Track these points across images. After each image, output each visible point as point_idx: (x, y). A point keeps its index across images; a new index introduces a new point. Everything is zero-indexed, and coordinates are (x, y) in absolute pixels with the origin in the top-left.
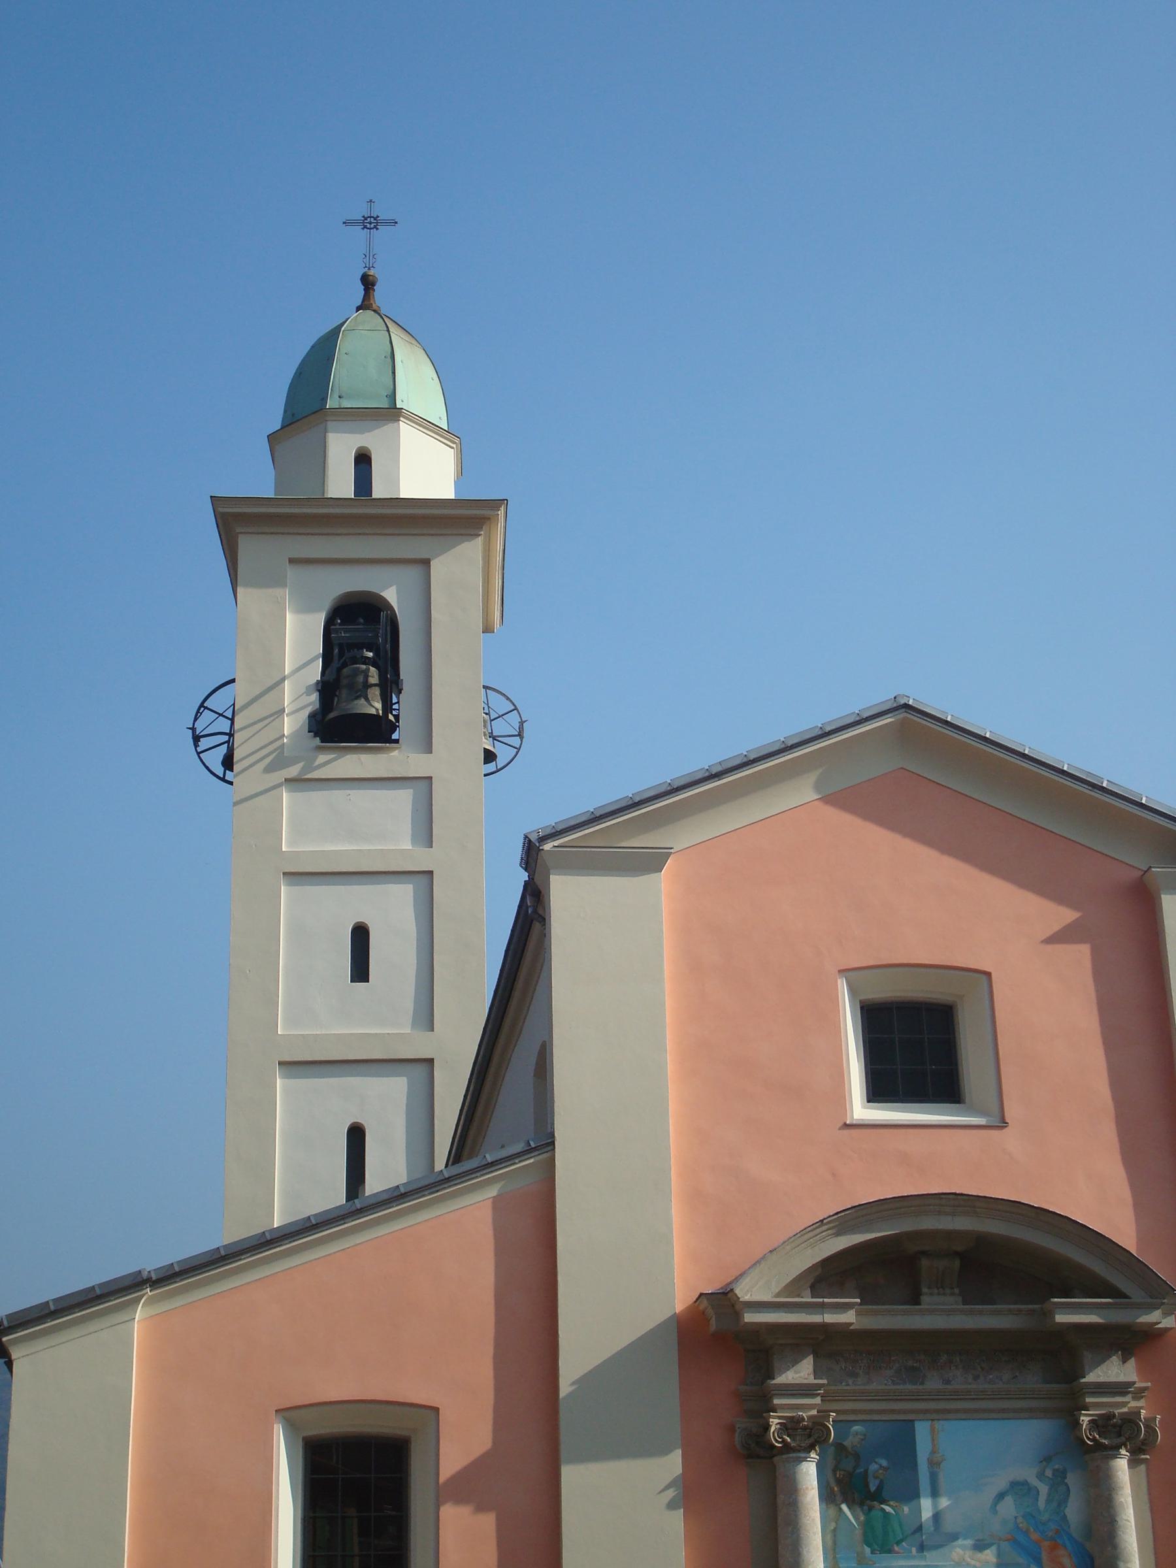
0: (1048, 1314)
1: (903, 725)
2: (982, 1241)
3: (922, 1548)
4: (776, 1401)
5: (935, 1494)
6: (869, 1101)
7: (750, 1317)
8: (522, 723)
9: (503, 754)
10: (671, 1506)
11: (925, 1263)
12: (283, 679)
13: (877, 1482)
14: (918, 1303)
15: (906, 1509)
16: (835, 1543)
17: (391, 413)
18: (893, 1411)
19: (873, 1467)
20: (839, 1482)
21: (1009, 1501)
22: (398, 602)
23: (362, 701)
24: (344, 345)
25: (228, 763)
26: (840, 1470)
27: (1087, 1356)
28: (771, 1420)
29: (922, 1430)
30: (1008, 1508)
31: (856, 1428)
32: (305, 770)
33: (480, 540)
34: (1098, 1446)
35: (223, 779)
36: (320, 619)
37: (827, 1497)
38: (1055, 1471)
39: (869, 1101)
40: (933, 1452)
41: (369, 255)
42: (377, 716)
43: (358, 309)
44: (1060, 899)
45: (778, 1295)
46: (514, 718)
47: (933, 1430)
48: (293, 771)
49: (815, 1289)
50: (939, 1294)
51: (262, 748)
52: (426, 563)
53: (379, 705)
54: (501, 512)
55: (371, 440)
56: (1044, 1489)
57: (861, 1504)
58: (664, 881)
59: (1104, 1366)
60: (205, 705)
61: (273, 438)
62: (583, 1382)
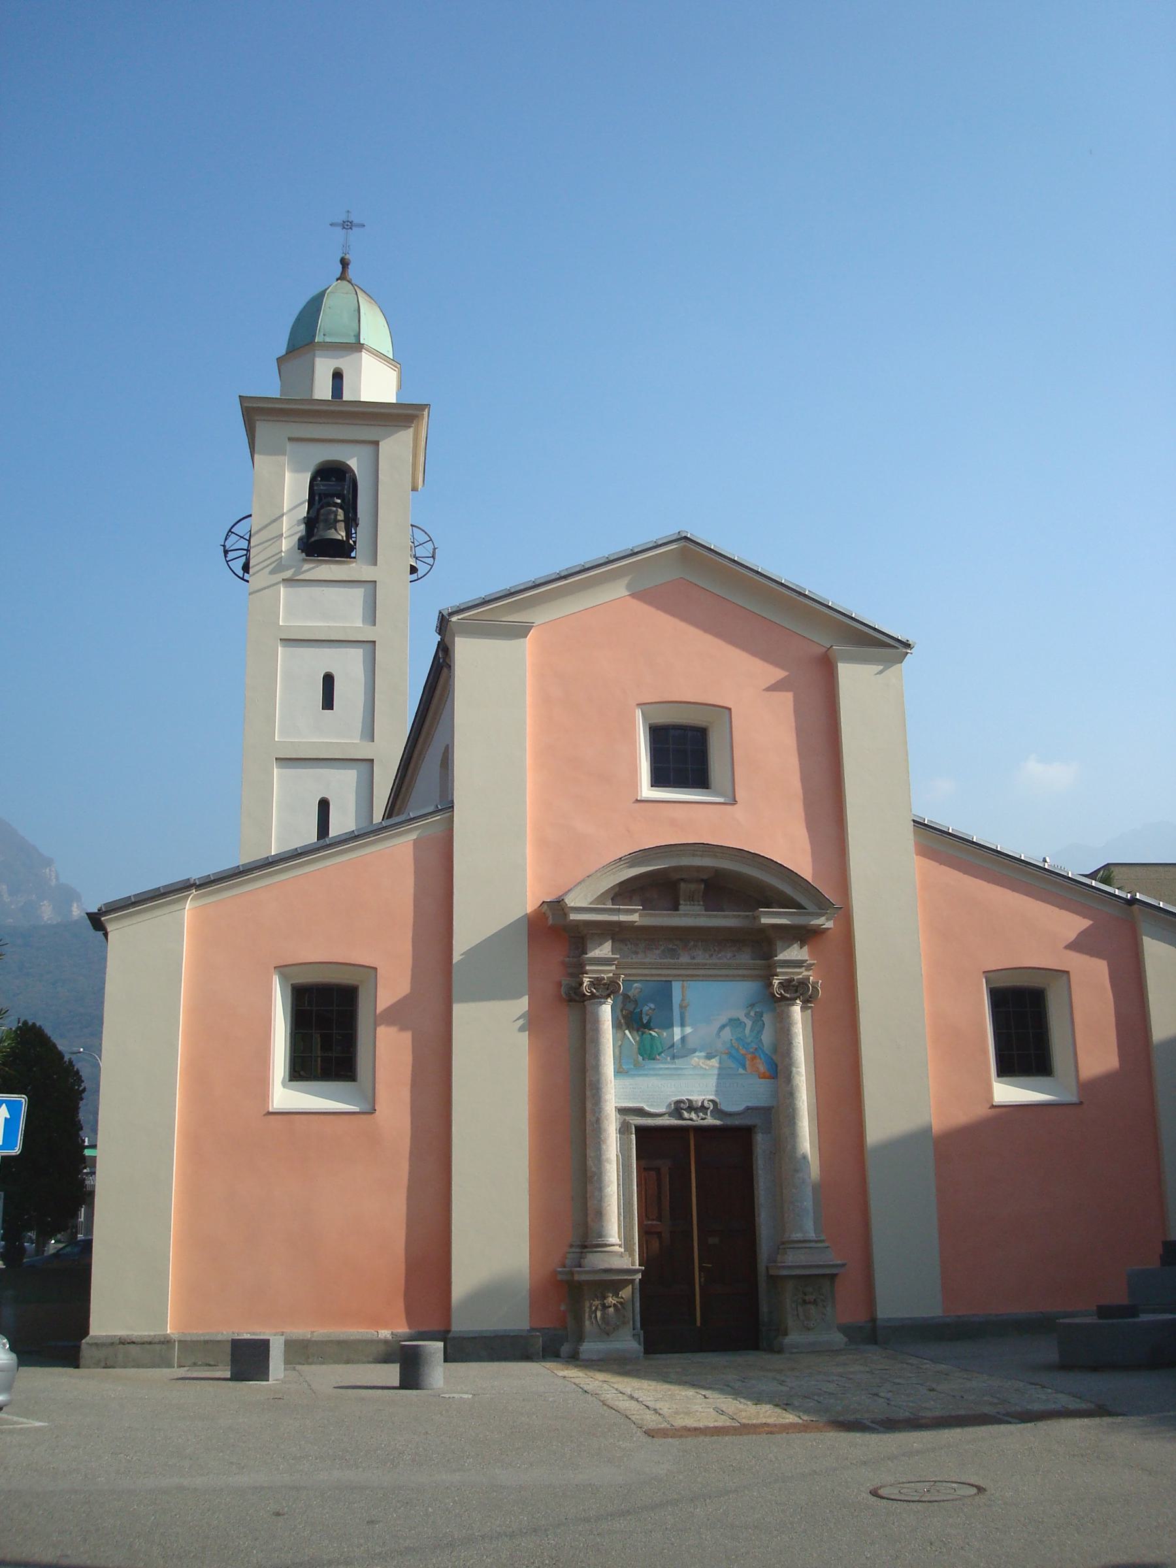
1: (683, 549)
2: (718, 874)
3: (674, 1057)
5: (683, 1025)
7: (573, 917)
8: (435, 549)
9: (422, 568)
10: (521, 1029)
11: (683, 885)
12: (283, 515)
13: (647, 1017)
14: (676, 909)
15: (665, 1034)
16: (620, 1053)
17: (356, 346)
19: (646, 1009)
20: (624, 1017)
21: (727, 1030)
25: (246, 568)
26: (626, 1010)
27: (779, 944)
28: (584, 979)
29: (676, 987)
30: (727, 1034)
31: (636, 985)
32: (295, 574)
33: (411, 430)
34: (783, 998)
37: (617, 1025)
40: (683, 1000)
41: (346, 246)
42: (342, 541)
44: (777, 664)
46: (429, 546)
47: (683, 987)
48: (288, 574)
50: (690, 905)
52: (376, 443)
53: (344, 534)
54: (426, 413)
56: (749, 1023)
57: (638, 1031)
58: (528, 644)
60: (232, 530)
62: (470, 954)
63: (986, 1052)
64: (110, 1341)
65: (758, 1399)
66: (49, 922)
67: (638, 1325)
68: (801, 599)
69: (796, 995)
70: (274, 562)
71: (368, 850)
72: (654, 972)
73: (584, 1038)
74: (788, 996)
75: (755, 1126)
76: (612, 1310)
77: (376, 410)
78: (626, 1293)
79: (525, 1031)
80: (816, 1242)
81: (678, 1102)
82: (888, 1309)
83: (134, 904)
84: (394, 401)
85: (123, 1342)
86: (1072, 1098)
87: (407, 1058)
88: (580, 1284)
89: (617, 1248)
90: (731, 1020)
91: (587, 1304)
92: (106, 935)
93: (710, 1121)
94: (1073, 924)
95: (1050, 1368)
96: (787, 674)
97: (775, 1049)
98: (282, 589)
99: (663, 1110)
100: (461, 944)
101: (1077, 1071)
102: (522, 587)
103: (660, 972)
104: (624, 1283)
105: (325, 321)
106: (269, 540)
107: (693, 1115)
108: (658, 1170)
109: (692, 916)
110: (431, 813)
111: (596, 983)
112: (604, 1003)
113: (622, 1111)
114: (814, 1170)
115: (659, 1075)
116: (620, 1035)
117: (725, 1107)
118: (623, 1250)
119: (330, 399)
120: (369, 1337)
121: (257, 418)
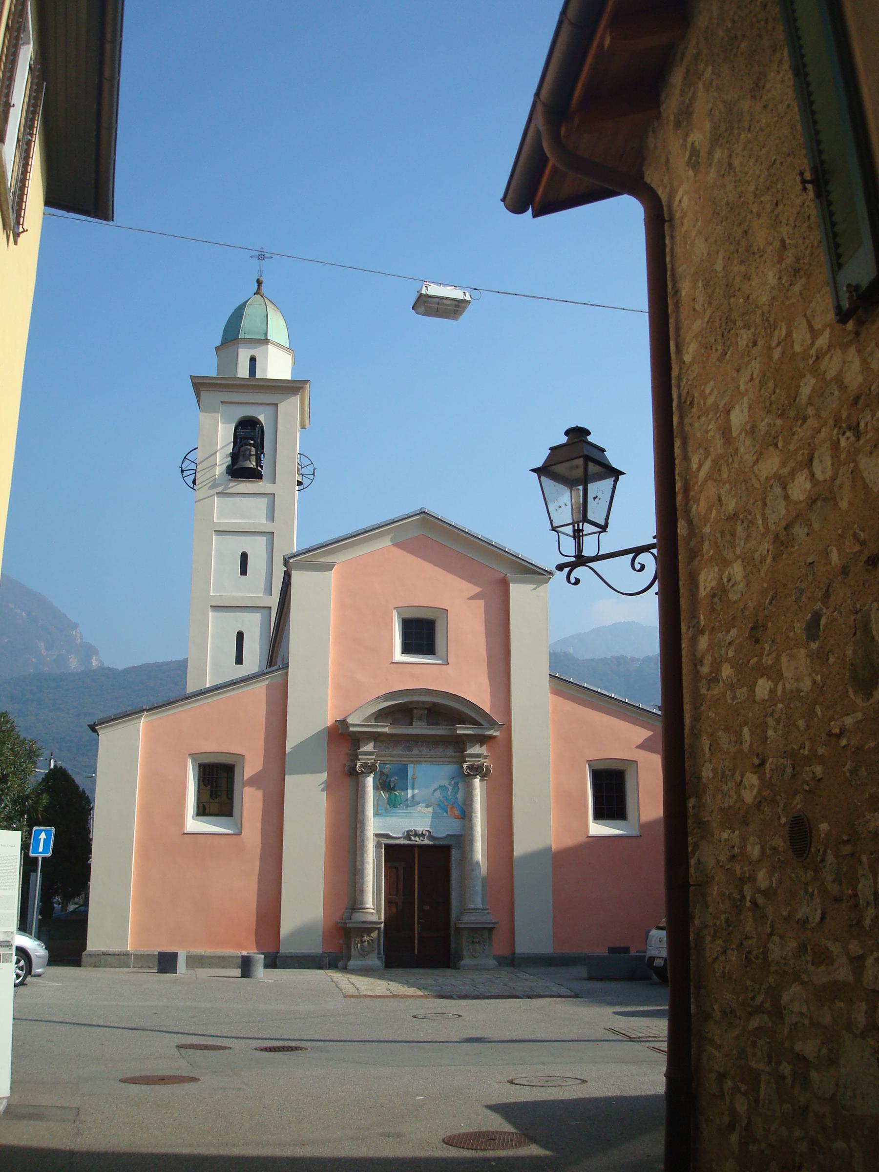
0: (455, 730)
1: (423, 519)
2: (435, 704)
3: (407, 806)
4: (360, 757)
5: (413, 788)
6: (402, 653)
7: (351, 729)
8: (314, 469)
9: (306, 482)
10: (322, 790)
11: (415, 711)
12: (217, 452)
14: (412, 725)
15: (403, 794)
16: (378, 804)
17: (265, 341)
18: (400, 761)
19: (393, 779)
20: (380, 784)
21: (438, 791)
22: (265, 420)
23: (248, 462)
24: (247, 311)
25: (194, 482)
27: (468, 744)
29: (410, 768)
30: (438, 794)
31: (387, 766)
32: (224, 489)
33: (299, 396)
34: (469, 775)
35: (193, 488)
36: (233, 426)
37: (376, 788)
38: (455, 782)
39: (402, 653)
41: (260, 272)
42: (254, 468)
43: (255, 294)
44: (476, 584)
45: (362, 722)
46: (311, 468)
47: (414, 767)
48: (220, 489)
49: (376, 719)
51: (207, 479)
52: (276, 405)
53: (254, 464)
54: (308, 386)
55: (256, 352)
56: (450, 788)
57: (388, 791)
58: (333, 574)
59: (473, 748)
61: (217, 349)
62: (294, 748)
63: (586, 806)
64: (97, 953)
65: (410, 985)
66: (75, 670)
67: (382, 952)
68: (490, 547)
69: (476, 773)
70: (209, 483)
71: (241, 690)
72: (398, 759)
73: (357, 795)
74: (472, 773)
75: (451, 845)
76: (366, 943)
77: (274, 384)
78: (374, 935)
79: (324, 791)
80: (482, 910)
81: (408, 831)
82: (522, 947)
83: (113, 720)
84: (290, 379)
85: (104, 954)
86: (635, 832)
87: (260, 805)
88: (350, 929)
89: (372, 911)
90: (440, 786)
91: (353, 940)
92: (98, 734)
93: (427, 842)
94: (642, 734)
95: (585, 979)
96: (481, 589)
97: (464, 803)
98: (216, 499)
99: (400, 835)
100: (291, 743)
101: (639, 817)
102: (330, 542)
103: (400, 759)
104: (373, 929)
105: (246, 323)
106: (209, 467)
107: (417, 839)
108: (397, 869)
109: (419, 728)
110: (278, 670)
111: (364, 765)
112: (368, 776)
113: (377, 836)
114: (484, 869)
115: (398, 816)
116: (378, 794)
117: (434, 834)
118: (375, 911)
119: (248, 377)
120: (235, 955)
121: (201, 389)
